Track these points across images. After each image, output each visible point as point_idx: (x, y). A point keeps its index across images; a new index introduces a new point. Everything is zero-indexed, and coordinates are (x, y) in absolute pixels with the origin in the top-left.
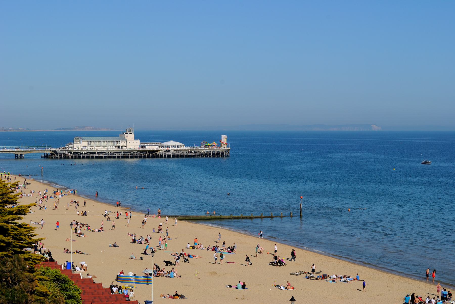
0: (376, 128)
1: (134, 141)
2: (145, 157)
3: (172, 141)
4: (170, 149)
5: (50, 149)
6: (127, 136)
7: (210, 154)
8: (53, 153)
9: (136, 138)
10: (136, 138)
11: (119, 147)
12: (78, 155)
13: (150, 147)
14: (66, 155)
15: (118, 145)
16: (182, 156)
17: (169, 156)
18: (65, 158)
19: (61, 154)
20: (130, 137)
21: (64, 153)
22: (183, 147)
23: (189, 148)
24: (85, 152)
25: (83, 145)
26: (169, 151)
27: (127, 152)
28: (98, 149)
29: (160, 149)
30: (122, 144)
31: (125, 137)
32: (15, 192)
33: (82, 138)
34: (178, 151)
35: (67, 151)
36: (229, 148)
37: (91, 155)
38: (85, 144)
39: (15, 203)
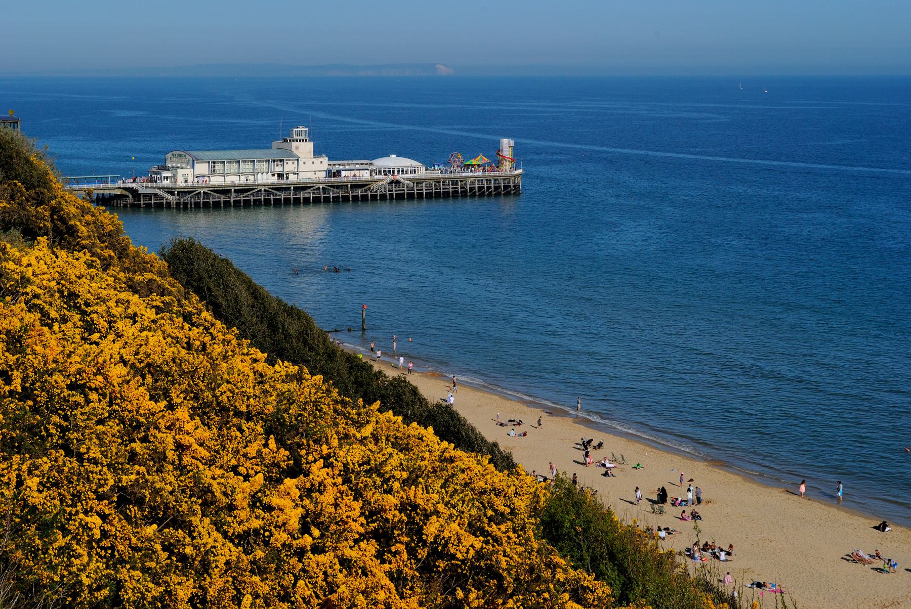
0: (443, 70)
1: (314, 160)
2: (346, 199)
3: (394, 156)
4: (399, 177)
5: (120, 184)
6: (297, 148)
8: (125, 193)
9: (317, 152)
10: (317, 152)
13: (354, 172)
14: (162, 198)
15: (278, 169)
16: (429, 196)
17: (400, 195)
18: (159, 206)
19: (147, 196)
20: (304, 149)
21: (156, 195)
22: (422, 172)
23: (436, 174)
24: (205, 190)
25: (197, 172)
26: (398, 182)
27: (304, 188)
28: (237, 182)
29: (377, 177)
30: (289, 167)
31: (293, 150)
32: (168, 354)
33: (194, 153)
34: (419, 182)
35: (162, 188)
36: (520, 171)
37: (223, 198)
38: (202, 168)
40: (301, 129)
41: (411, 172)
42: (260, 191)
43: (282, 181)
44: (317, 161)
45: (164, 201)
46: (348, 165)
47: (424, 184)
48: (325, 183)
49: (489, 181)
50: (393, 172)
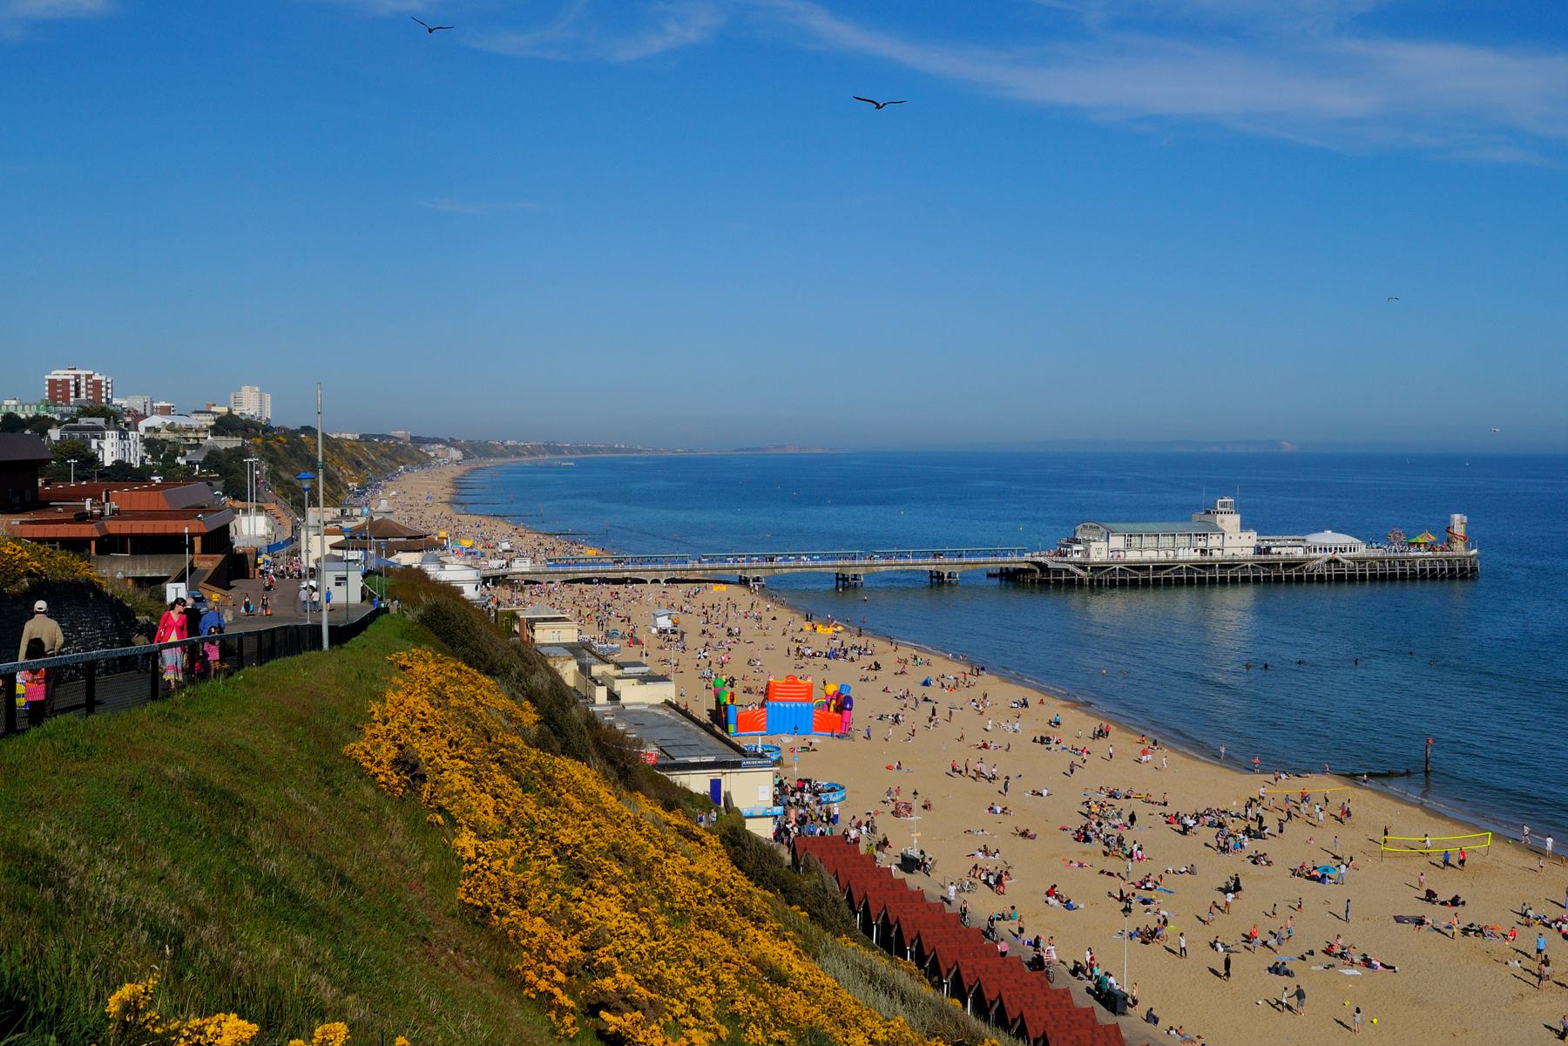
4: (1338, 555)
7: (1442, 570)
9: (1244, 527)
10: (1244, 527)
11: (1203, 551)
12: (1108, 580)
15: (1201, 544)
17: (1339, 577)
19: (1058, 572)
21: (1067, 570)
26: (1336, 561)
29: (1312, 555)
30: (1214, 541)
33: (1108, 525)
36: (1475, 551)
37: (1141, 575)
38: (1117, 542)
39: (485, 580)
44: (1245, 535)
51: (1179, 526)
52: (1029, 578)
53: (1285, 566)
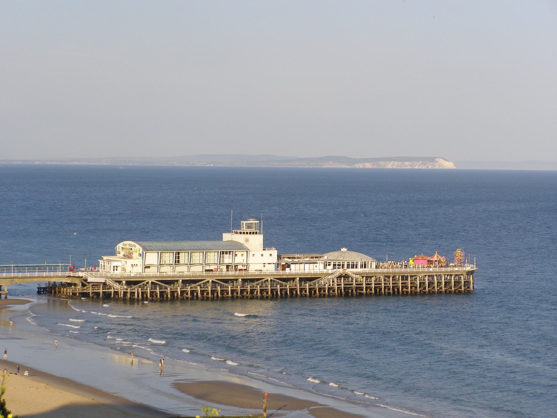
4: (349, 271)
9: (267, 245)
10: (267, 245)
17: (349, 292)
26: (346, 276)
40: (252, 221)
41: (362, 267)
42: (267, 280)
43: (230, 273)
44: (267, 253)
45: (112, 290)
46: (298, 258)
47: (373, 279)
48: (273, 275)
49: (405, 278)
50: (343, 266)
51: (208, 244)
52: (70, 291)
53: (301, 280)
